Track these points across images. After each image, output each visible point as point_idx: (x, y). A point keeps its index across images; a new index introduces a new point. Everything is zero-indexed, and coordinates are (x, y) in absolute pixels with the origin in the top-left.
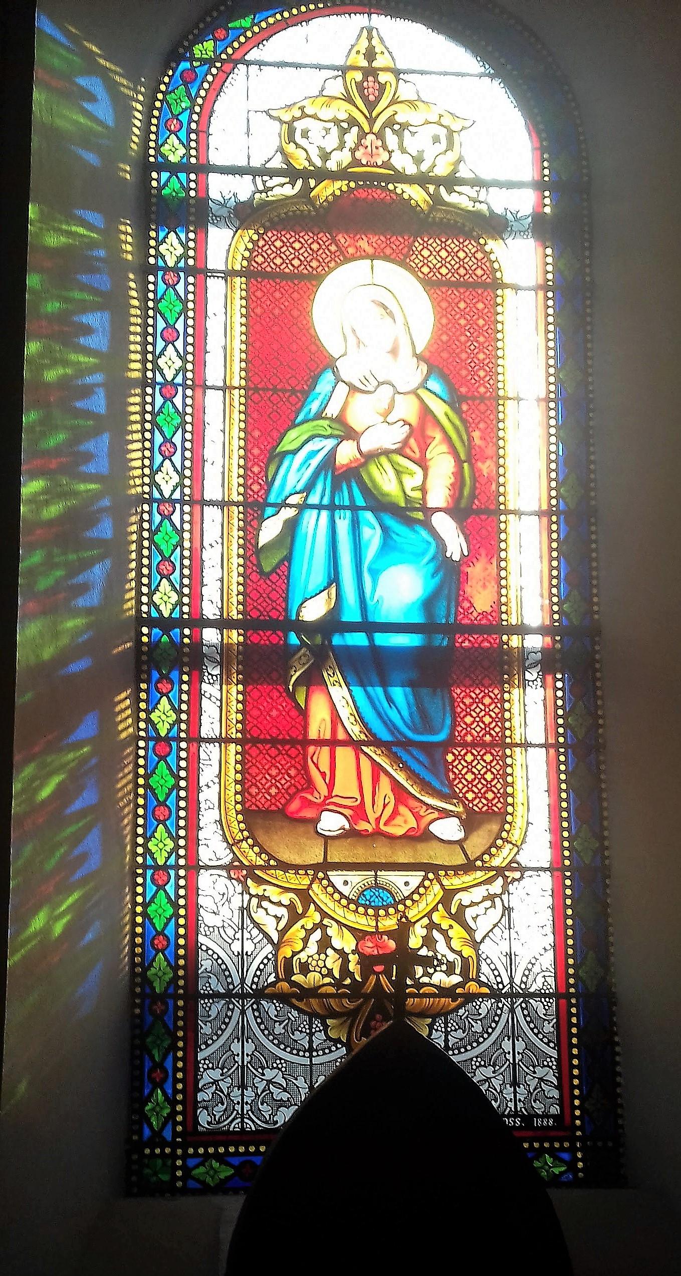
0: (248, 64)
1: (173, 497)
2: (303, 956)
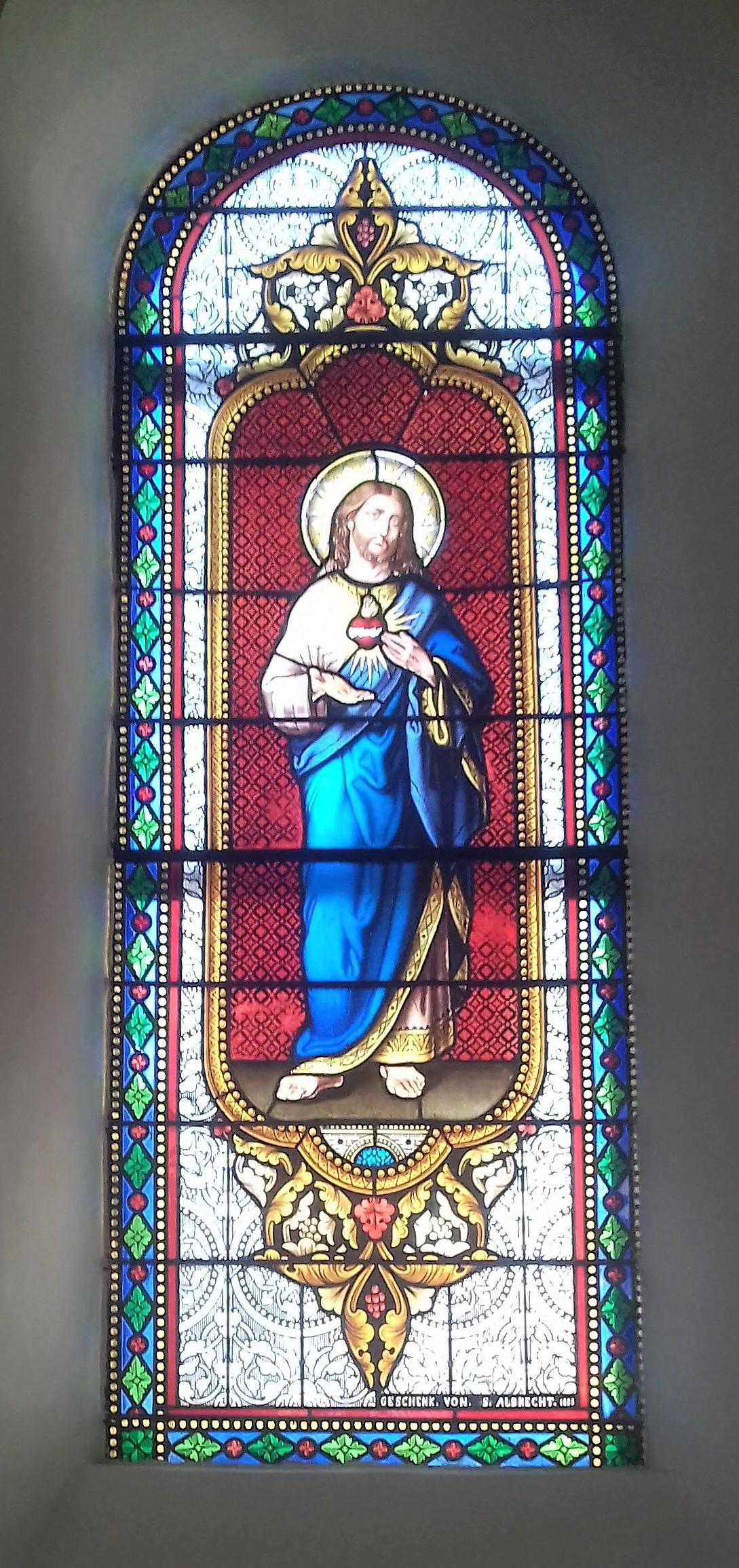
0: (226, 212)
1: (145, 1119)
2: (293, 1223)
